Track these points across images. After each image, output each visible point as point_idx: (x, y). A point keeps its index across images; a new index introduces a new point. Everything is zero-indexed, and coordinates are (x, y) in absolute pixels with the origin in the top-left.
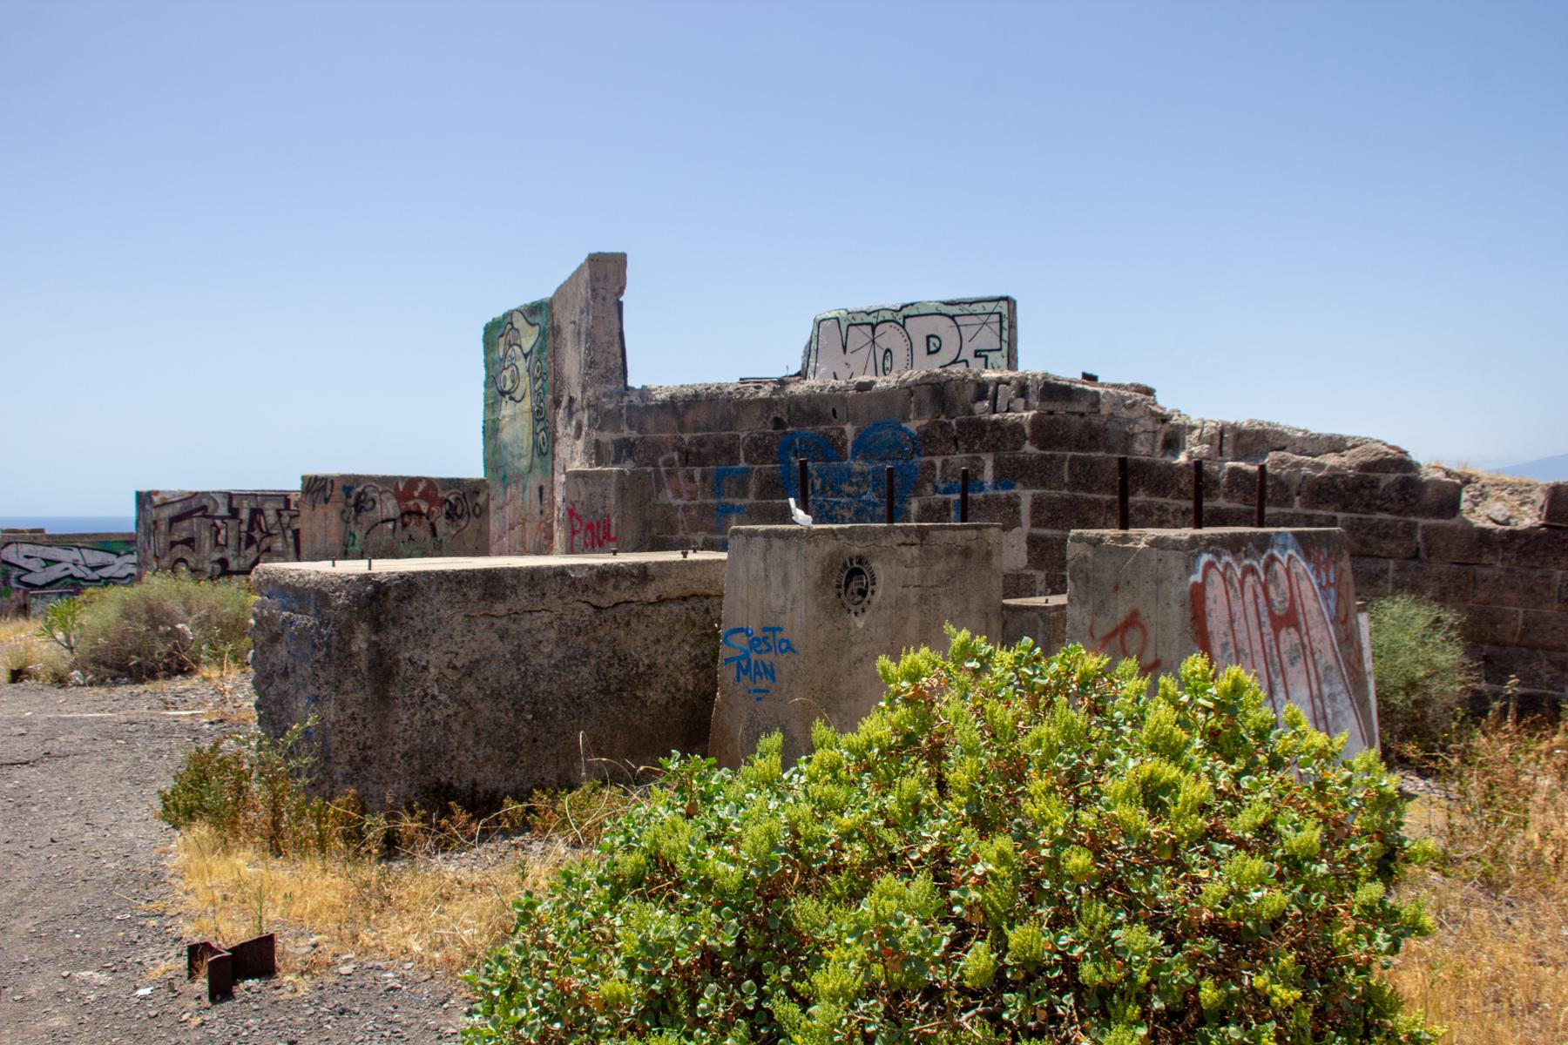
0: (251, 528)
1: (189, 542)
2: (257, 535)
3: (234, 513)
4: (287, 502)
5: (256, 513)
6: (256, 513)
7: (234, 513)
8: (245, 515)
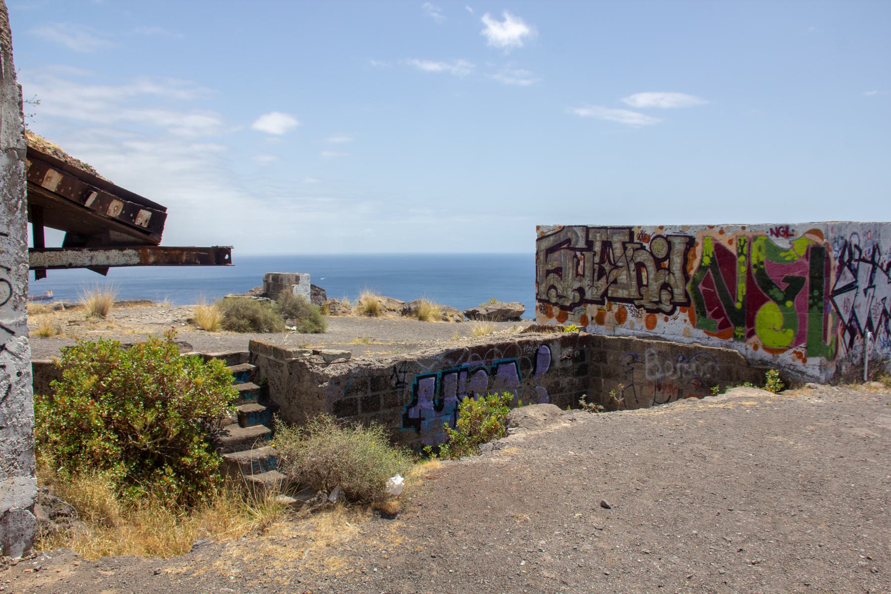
0: (602, 261)
1: (558, 271)
2: (607, 267)
3: (590, 245)
4: (631, 234)
5: (607, 245)
6: (607, 245)
7: (590, 245)
8: (597, 247)
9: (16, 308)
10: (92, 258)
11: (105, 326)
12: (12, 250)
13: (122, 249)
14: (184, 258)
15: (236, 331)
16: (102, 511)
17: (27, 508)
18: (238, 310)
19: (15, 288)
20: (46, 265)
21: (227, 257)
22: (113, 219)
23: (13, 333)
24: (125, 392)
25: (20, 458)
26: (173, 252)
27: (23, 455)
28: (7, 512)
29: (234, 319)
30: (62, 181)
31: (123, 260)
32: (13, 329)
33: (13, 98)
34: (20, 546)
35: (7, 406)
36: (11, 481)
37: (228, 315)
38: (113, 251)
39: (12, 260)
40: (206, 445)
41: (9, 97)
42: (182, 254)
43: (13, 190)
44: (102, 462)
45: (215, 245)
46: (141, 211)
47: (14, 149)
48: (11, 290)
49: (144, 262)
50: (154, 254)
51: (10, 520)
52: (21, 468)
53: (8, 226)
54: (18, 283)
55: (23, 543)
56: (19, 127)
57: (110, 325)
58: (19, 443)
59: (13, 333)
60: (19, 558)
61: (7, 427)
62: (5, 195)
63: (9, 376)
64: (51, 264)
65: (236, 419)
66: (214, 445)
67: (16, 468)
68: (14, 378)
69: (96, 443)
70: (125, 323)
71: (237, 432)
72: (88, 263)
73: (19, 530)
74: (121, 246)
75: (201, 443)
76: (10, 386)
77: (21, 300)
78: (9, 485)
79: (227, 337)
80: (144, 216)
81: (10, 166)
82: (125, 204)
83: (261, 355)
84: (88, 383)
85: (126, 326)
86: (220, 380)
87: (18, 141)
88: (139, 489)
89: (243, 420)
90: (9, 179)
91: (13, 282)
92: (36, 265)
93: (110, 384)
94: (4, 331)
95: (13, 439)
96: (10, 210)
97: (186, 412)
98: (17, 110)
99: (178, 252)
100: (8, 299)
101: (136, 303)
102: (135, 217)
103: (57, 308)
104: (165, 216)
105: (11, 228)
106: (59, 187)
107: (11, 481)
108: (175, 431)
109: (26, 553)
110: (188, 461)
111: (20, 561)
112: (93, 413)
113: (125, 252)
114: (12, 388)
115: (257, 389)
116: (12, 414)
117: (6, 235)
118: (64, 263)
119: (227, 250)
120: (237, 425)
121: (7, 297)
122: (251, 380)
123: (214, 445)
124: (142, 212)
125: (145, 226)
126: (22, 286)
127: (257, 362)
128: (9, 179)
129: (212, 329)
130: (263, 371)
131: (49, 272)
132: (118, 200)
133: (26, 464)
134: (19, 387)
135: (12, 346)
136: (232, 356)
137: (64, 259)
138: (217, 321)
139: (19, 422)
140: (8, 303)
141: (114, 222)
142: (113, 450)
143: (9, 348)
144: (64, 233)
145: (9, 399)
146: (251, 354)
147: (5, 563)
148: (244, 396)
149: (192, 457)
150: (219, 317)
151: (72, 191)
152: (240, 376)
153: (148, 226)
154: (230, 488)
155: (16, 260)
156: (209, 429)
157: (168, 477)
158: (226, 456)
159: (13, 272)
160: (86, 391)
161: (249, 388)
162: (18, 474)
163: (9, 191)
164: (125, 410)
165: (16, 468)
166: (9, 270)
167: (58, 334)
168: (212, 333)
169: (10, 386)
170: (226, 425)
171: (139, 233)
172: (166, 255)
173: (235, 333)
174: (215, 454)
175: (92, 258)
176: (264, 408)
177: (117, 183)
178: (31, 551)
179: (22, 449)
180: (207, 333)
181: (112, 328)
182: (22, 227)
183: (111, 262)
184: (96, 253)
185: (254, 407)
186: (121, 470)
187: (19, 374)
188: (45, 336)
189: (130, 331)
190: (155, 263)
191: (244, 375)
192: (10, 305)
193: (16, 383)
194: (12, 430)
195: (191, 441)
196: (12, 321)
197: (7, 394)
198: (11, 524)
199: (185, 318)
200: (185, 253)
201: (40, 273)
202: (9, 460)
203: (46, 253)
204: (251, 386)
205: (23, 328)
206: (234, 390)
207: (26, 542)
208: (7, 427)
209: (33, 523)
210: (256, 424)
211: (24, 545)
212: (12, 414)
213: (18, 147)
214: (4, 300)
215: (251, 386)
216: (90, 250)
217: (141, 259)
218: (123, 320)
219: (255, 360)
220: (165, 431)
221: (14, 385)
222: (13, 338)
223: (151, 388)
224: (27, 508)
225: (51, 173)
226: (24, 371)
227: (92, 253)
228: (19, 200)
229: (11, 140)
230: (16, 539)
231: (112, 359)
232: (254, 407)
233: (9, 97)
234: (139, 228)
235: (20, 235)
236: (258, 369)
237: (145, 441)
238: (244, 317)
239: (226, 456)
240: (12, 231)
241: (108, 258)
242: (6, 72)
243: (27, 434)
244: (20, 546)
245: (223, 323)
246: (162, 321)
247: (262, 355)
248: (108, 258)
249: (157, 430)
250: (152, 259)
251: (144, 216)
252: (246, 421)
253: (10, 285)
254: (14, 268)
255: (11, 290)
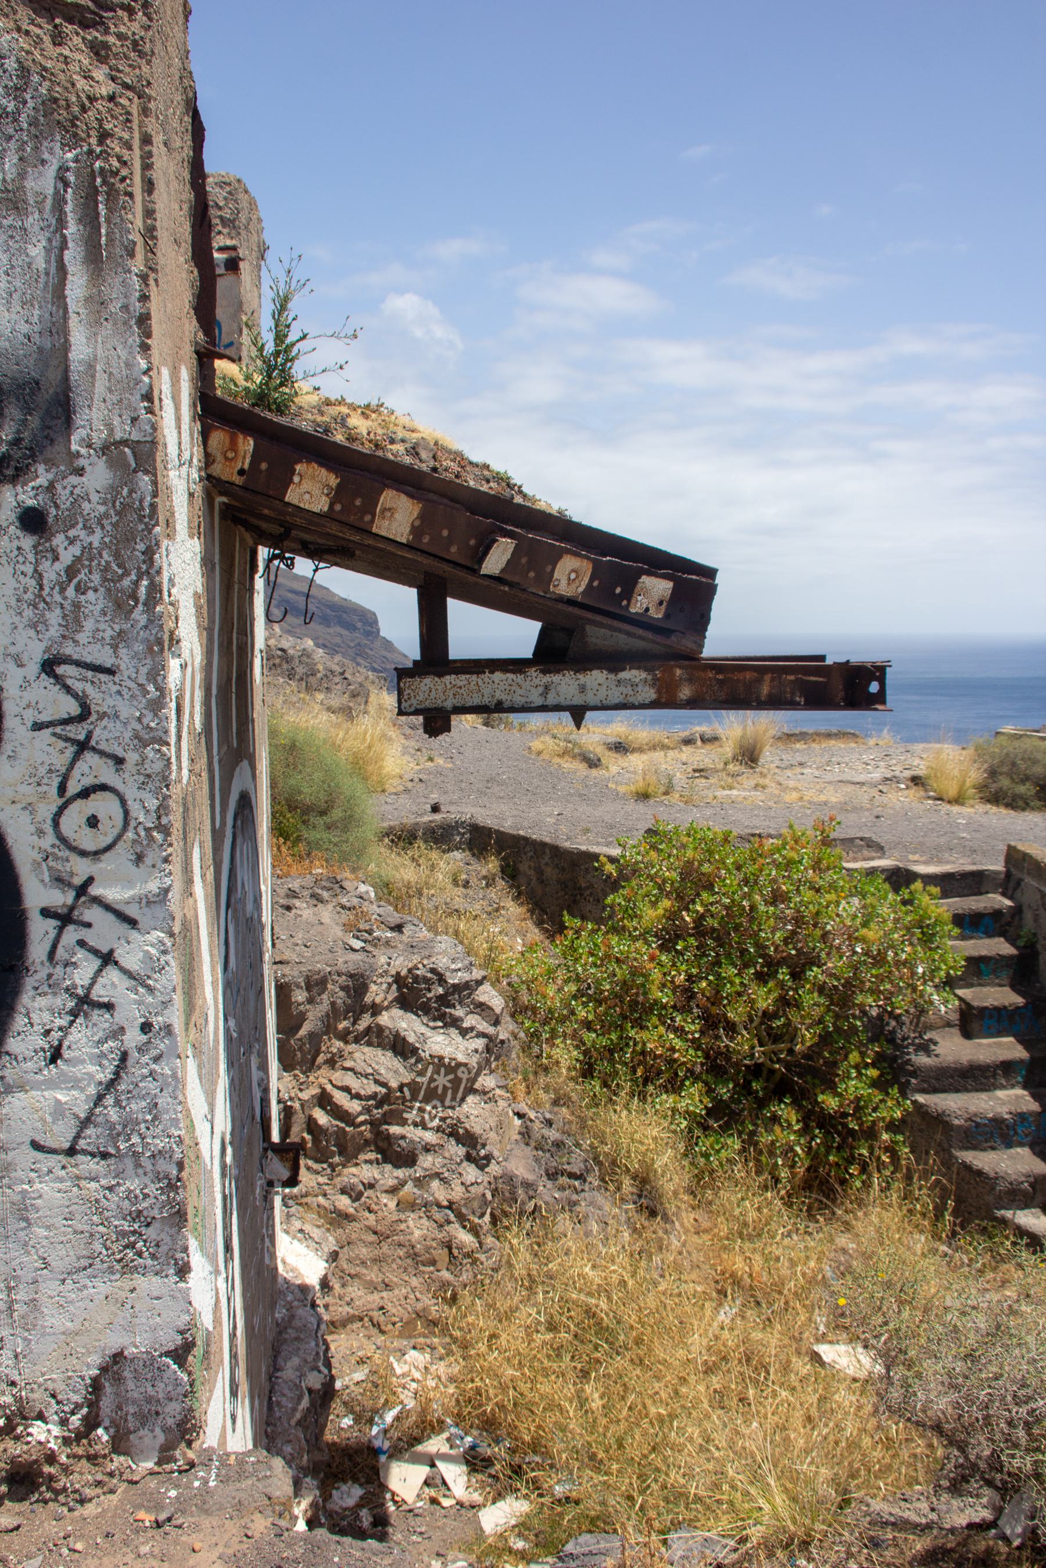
9: (139, 858)
10: (547, 688)
11: (753, 783)
12: (127, 710)
13: (614, 670)
14: (765, 690)
15: (1007, 806)
16: (644, 1181)
17: (167, 1354)
18: (1014, 764)
19: (134, 807)
20: (449, 705)
21: (874, 687)
22: (571, 602)
23: (132, 923)
24: (719, 938)
25: (151, 1233)
26: (738, 676)
27: (156, 1225)
28: (118, 1357)
29: (1005, 782)
30: (422, 516)
31: (616, 698)
32: (132, 911)
33: (125, 308)
34: (152, 1438)
35: (118, 1103)
36: (127, 1284)
37: (993, 773)
38: (596, 673)
39: (128, 735)
40: (873, 1073)
41: (115, 307)
42: (759, 681)
43: (126, 553)
44: (656, 1075)
45: (843, 660)
46: (644, 578)
47: (125, 442)
48: (126, 813)
49: (665, 701)
50: (690, 680)
51: (126, 1374)
52: (153, 1256)
53: (115, 647)
54: (145, 795)
55: (158, 1430)
56: (138, 382)
57: (761, 781)
58: (146, 1196)
59: (132, 923)
60: (150, 1464)
61: (119, 1156)
62: (107, 568)
63: (122, 1029)
64: (458, 702)
65: (954, 1017)
66: (894, 1073)
67: (140, 1254)
68: (133, 1037)
69: (653, 1038)
70: (790, 778)
71: (952, 1049)
72: (538, 701)
73: (149, 1400)
74: (613, 661)
75: (867, 1066)
76: (124, 1056)
77: (152, 839)
78: (123, 1294)
79: (984, 820)
80: (653, 592)
81: (114, 490)
82: (597, 566)
83: (1028, 880)
84: (652, 915)
85: (791, 784)
86: (925, 934)
87: (134, 420)
88: (729, 1141)
89: (971, 1022)
90: (115, 525)
91: (131, 793)
92: (427, 704)
93: (700, 919)
94: (111, 917)
95: (133, 1184)
96: (119, 605)
97: (840, 997)
98: (135, 340)
99: (748, 675)
100: (119, 837)
101: (829, 736)
102: (629, 593)
103: (688, 742)
104: (712, 589)
105: (123, 652)
106: (415, 531)
107: (129, 1285)
108: (808, 1037)
109: (165, 1456)
110: (830, 1102)
111: (152, 1473)
112: (656, 975)
113: (623, 675)
114: (130, 1062)
115: (1011, 957)
116: (129, 1125)
117: (110, 672)
118: (486, 700)
119: (878, 672)
120: (956, 1031)
121: (116, 832)
122: (1002, 934)
123: (894, 1073)
124: (647, 581)
125: (657, 614)
126: (153, 803)
127: (1018, 894)
128: (115, 525)
129: (958, 800)
130: (1028, 916)
131: (455, 720)
132: (576, 555)
133: (164, 1248)
134: (145, 1059)
135: (130, 958)
136: (965, 876)
137: (487, 691)
138: (968, 783)
139: (145, 1146)
140: (120, 847)
141: (571, 609)
142: (687, 1056)
143: (124, 962)
144: (537, 626)
145: (122, 1087)
146: (1008, 874)
147: (111, 1474)
148: (978, 968)
149: (840, 1095)
150: (976, 775)
151: (450, 540)
152: (970, 924)
153: (667, 616)
154: (909, 1178)
155: (137, 736)
156: (893, 1032)
157: (786, 1129)
158: (921, 1098)
159: (129, 766)
160: (647, 932)
161: (992, 953)
162: (144, 1271)
163: (117, 555)
164: (718, 976)
165: (140, 1254)
166: (119, 761)
167: (666, 793)
168: (955, 809)
169: (124, 1056)
170: (931, 1027)
171: (649, 635)
172: (721, 682)
173: (1003, 811)
174: (894, 1091)
175: (547, 688)
176: (1020, 1000)
177: (581, 513)
178: (178, 1453)
179: (156, 1213)
180: (945, 807)
181: (764, 787)
182: (150, 650)
183: (591, 699)
184: (556, 678)
185: (999, 995)
186: (693, 1099)
187: (146, 1027)
188: (644, 796)
189: (795, 795)
190: (693, 703)
191: (986, 920)
192: (123, 853)
193: (140, 1050)
194: (129, 1163)
195: (846, 1058)
196: (128, 894)
197: (117, 1074)
198: (131, 1384)
199: (908, 774)
200: (767, 678)
201: (436, 722)
202: (123, 1234)
203: (449, 679)
204: (1000, 947)
205: (158, 911)
206: (958, 949)
207: (166, 1430)
208: (119, 1156)
209: (181, 1390)
210: (999, 1034)
211: (161, 1438)
212: (129, 1125)
213: (135, 436)
214: (109, 840)
215: (1000, 947)
216: (544, 672)
217: (659, 692)
218: (789, 773)
219: (1015, 889)
220: (789, 1034)
221: (134, 1055)
222: (134, 935)
223: (773, 936)
224: (167, 1354)
225: (389, 497)
226: (157, 1021)
227: (547, 678)
228: (140, 578)
229: (116, 421)
230: (144, 1419)
231: (706, 868)
232: (999, 995)
233: (115, 307)
234: (642, 622)
235: (144, 670)
236: (1017, 911)
237: (743, 1045)
238: (1026, 779)
239: (921, 1098)
240: (125, 661)
241: (583, 689)
242: (110, 240)
243: (167, 1177)
244: (152, 1438)
245: (981, 788)
246: (861, 778)
247: (1030, 881)
248: (583, 689)
249: (770, 1029)
250: (685, 692)
251: (653, 592)
252: (975, 1026)
253: (123, 802)
254: (132, 757)
255: (126, 813)
